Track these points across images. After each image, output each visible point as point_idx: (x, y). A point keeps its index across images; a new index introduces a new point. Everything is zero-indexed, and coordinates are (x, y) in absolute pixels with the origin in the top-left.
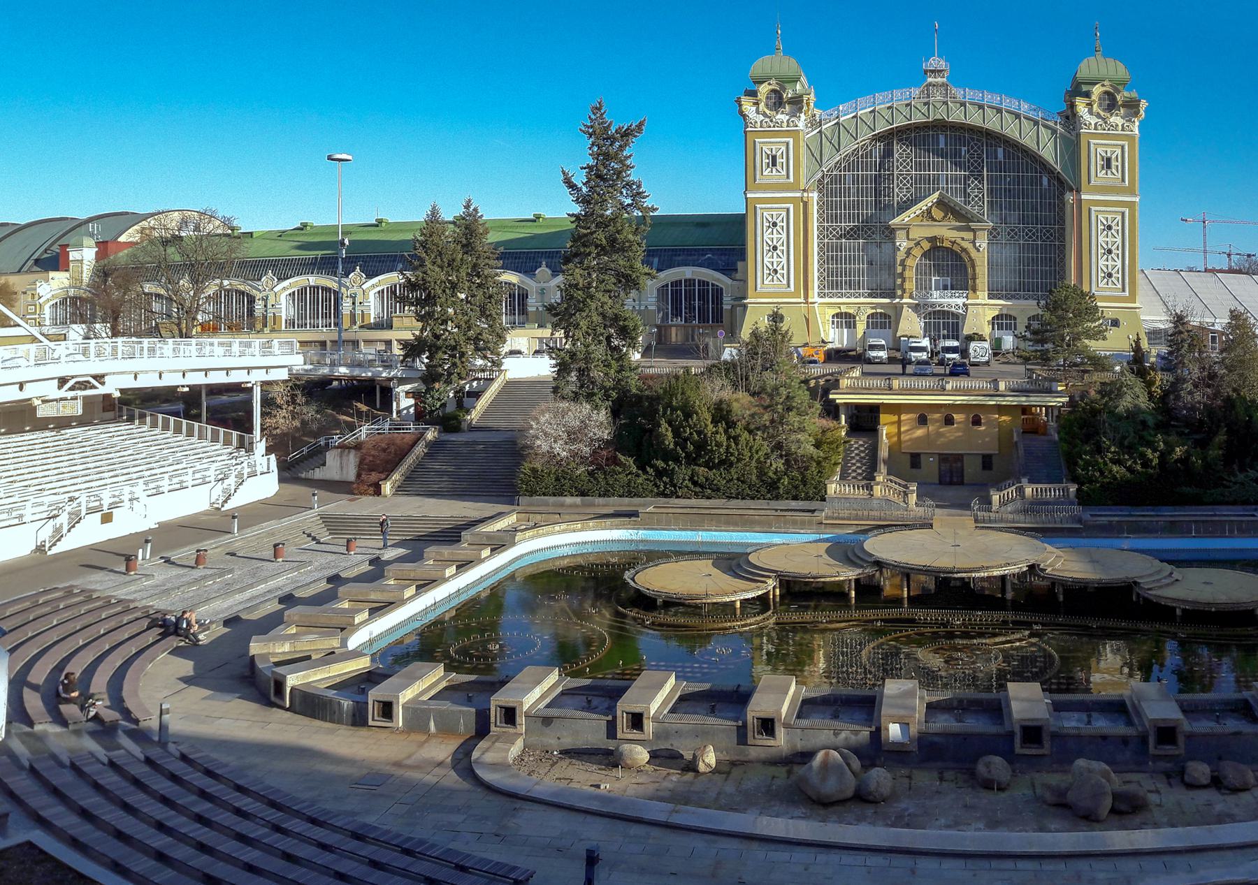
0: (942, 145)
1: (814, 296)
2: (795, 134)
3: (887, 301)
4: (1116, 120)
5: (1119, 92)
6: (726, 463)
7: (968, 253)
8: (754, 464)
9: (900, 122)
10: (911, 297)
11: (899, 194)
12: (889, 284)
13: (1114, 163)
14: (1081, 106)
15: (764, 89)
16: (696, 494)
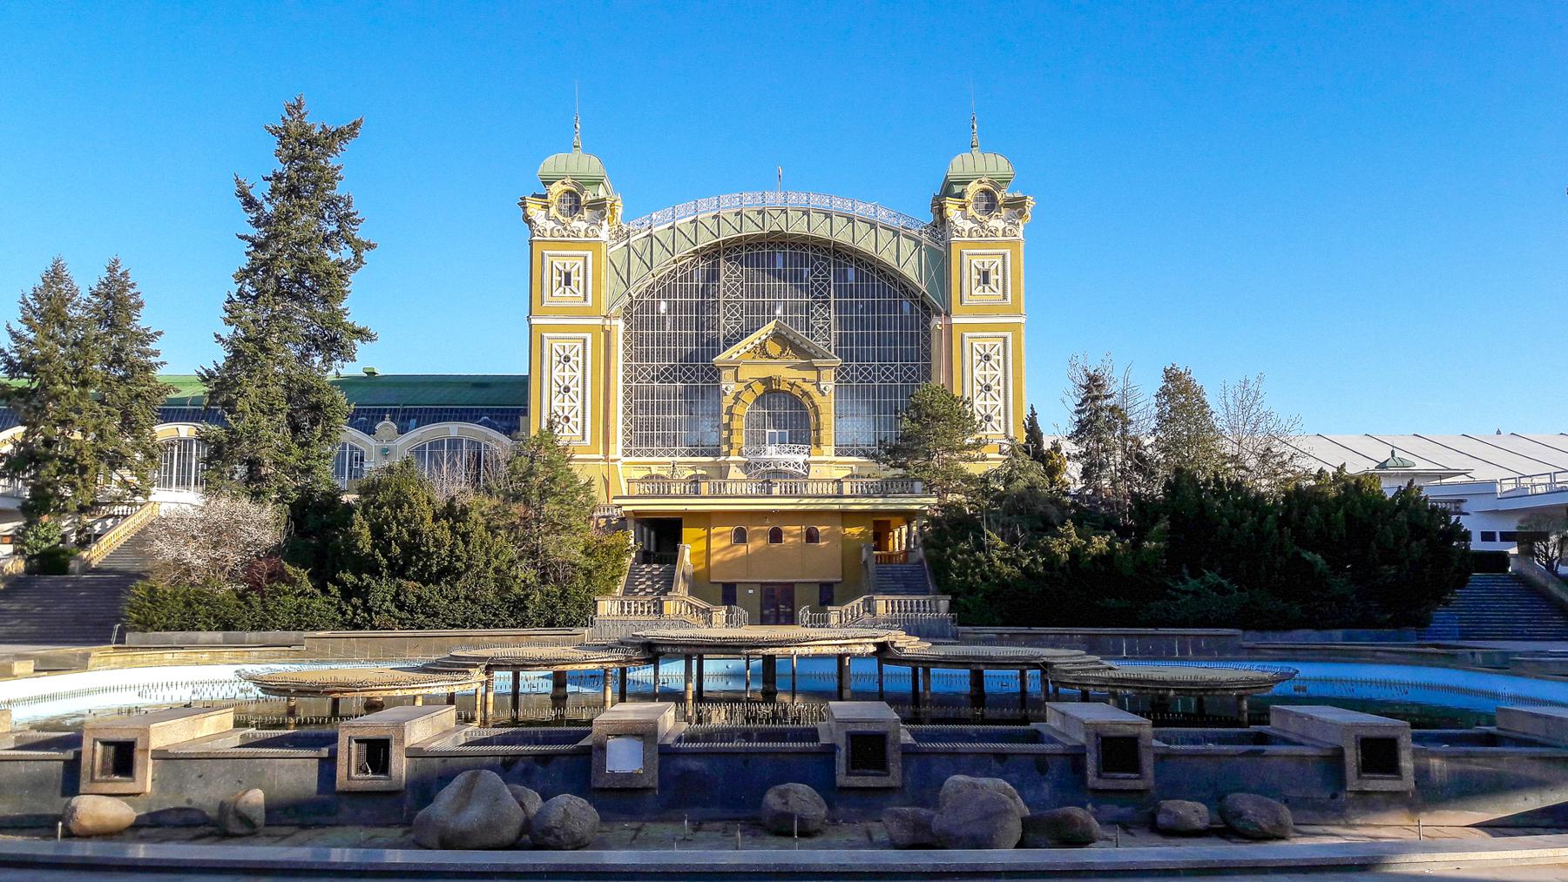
0: (779, 267)
1: (617, 449)
2: (596, 245)
3: (711, 459)
4: (996, 223)
5: (999, 189)
6: (449, 572)
7: (810, 397)
8: (491, 573)
9: (728, 233)
10: (740, 454)
11: (725, 324)
12: (713, 439)
13: (992, 277)
14: (952, 209)
15: (556, 189)
16: (402, 622)
